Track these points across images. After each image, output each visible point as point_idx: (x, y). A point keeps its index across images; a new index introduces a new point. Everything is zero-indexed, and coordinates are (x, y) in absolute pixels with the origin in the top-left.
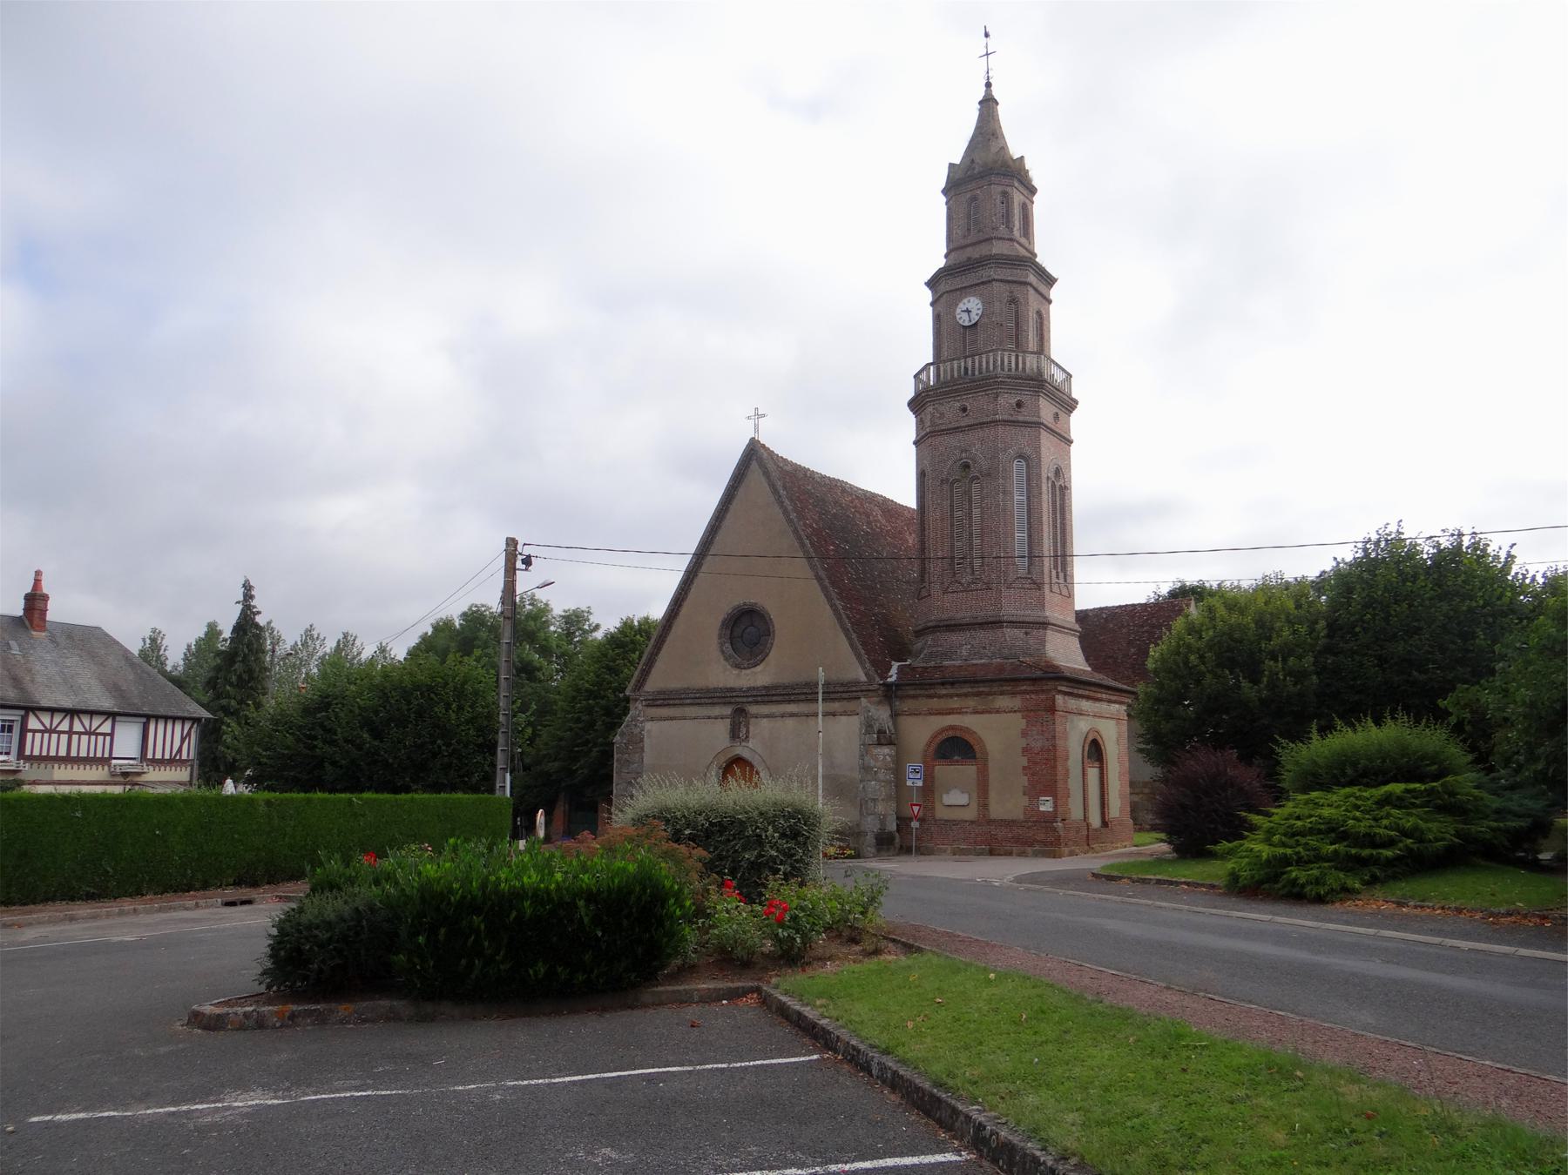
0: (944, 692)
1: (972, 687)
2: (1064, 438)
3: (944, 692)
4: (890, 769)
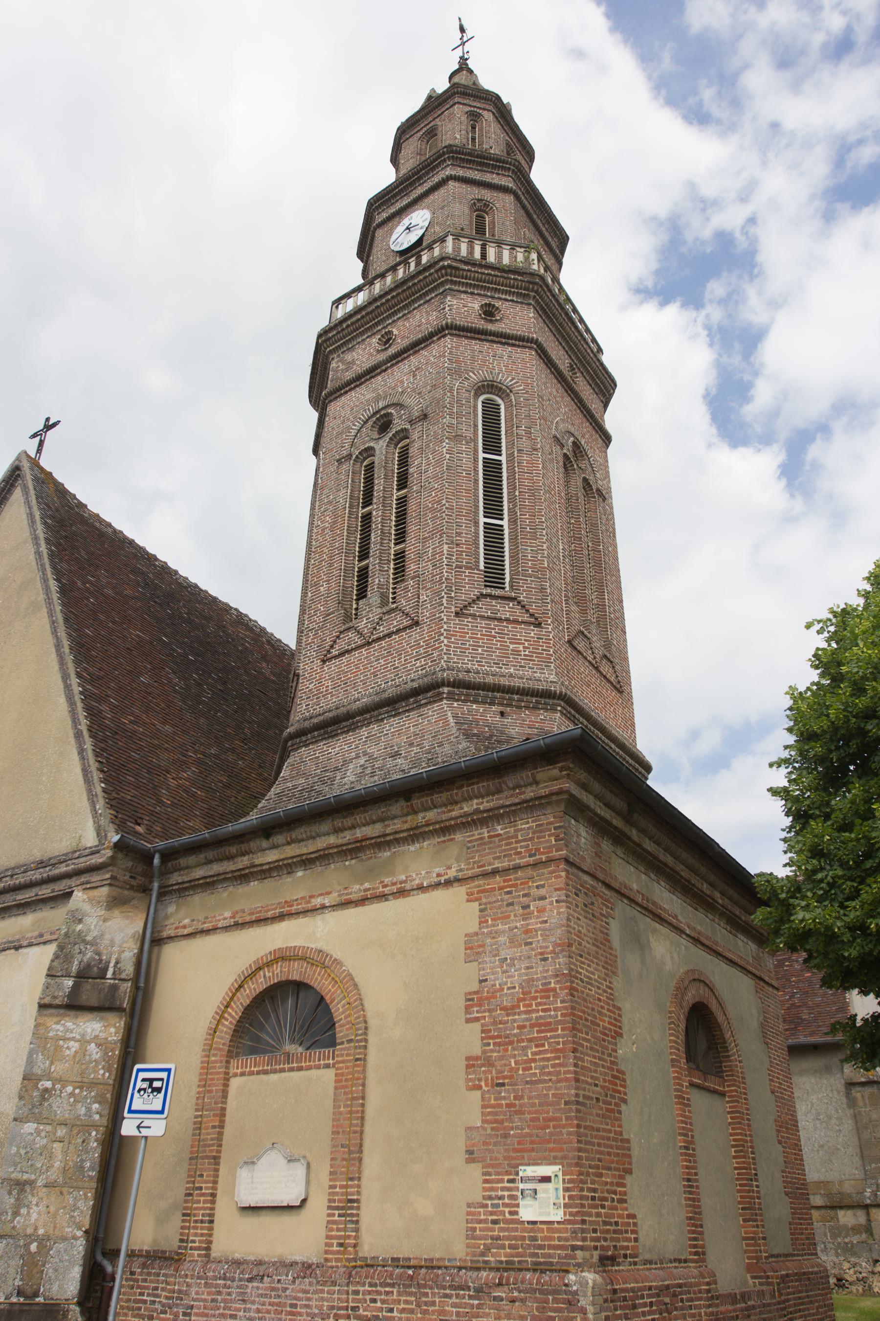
0: (272, 856)
1: (337, 831)
2: (592, 416)
3: (272, 856)
4: (92, 1085)
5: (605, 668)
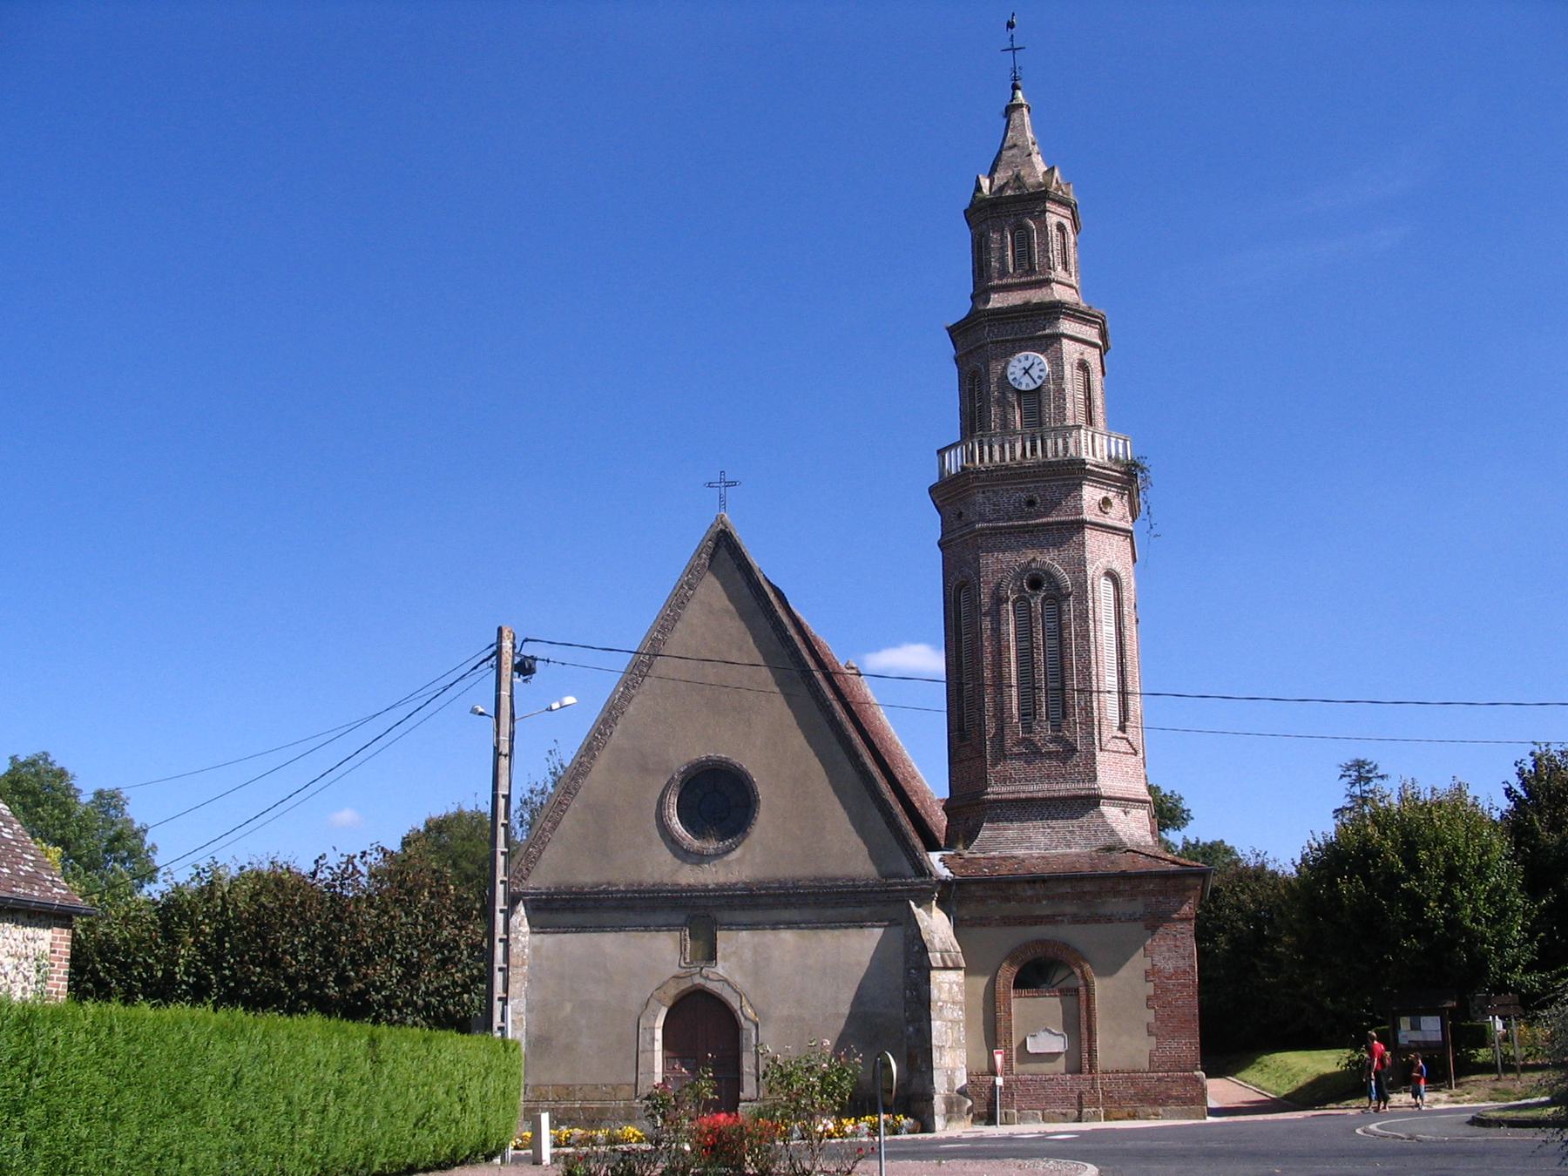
5: (1473, 1083)
